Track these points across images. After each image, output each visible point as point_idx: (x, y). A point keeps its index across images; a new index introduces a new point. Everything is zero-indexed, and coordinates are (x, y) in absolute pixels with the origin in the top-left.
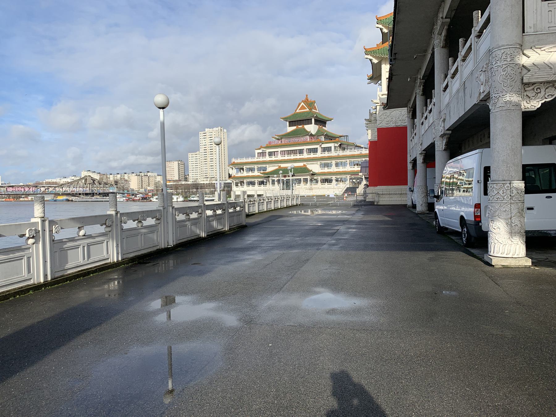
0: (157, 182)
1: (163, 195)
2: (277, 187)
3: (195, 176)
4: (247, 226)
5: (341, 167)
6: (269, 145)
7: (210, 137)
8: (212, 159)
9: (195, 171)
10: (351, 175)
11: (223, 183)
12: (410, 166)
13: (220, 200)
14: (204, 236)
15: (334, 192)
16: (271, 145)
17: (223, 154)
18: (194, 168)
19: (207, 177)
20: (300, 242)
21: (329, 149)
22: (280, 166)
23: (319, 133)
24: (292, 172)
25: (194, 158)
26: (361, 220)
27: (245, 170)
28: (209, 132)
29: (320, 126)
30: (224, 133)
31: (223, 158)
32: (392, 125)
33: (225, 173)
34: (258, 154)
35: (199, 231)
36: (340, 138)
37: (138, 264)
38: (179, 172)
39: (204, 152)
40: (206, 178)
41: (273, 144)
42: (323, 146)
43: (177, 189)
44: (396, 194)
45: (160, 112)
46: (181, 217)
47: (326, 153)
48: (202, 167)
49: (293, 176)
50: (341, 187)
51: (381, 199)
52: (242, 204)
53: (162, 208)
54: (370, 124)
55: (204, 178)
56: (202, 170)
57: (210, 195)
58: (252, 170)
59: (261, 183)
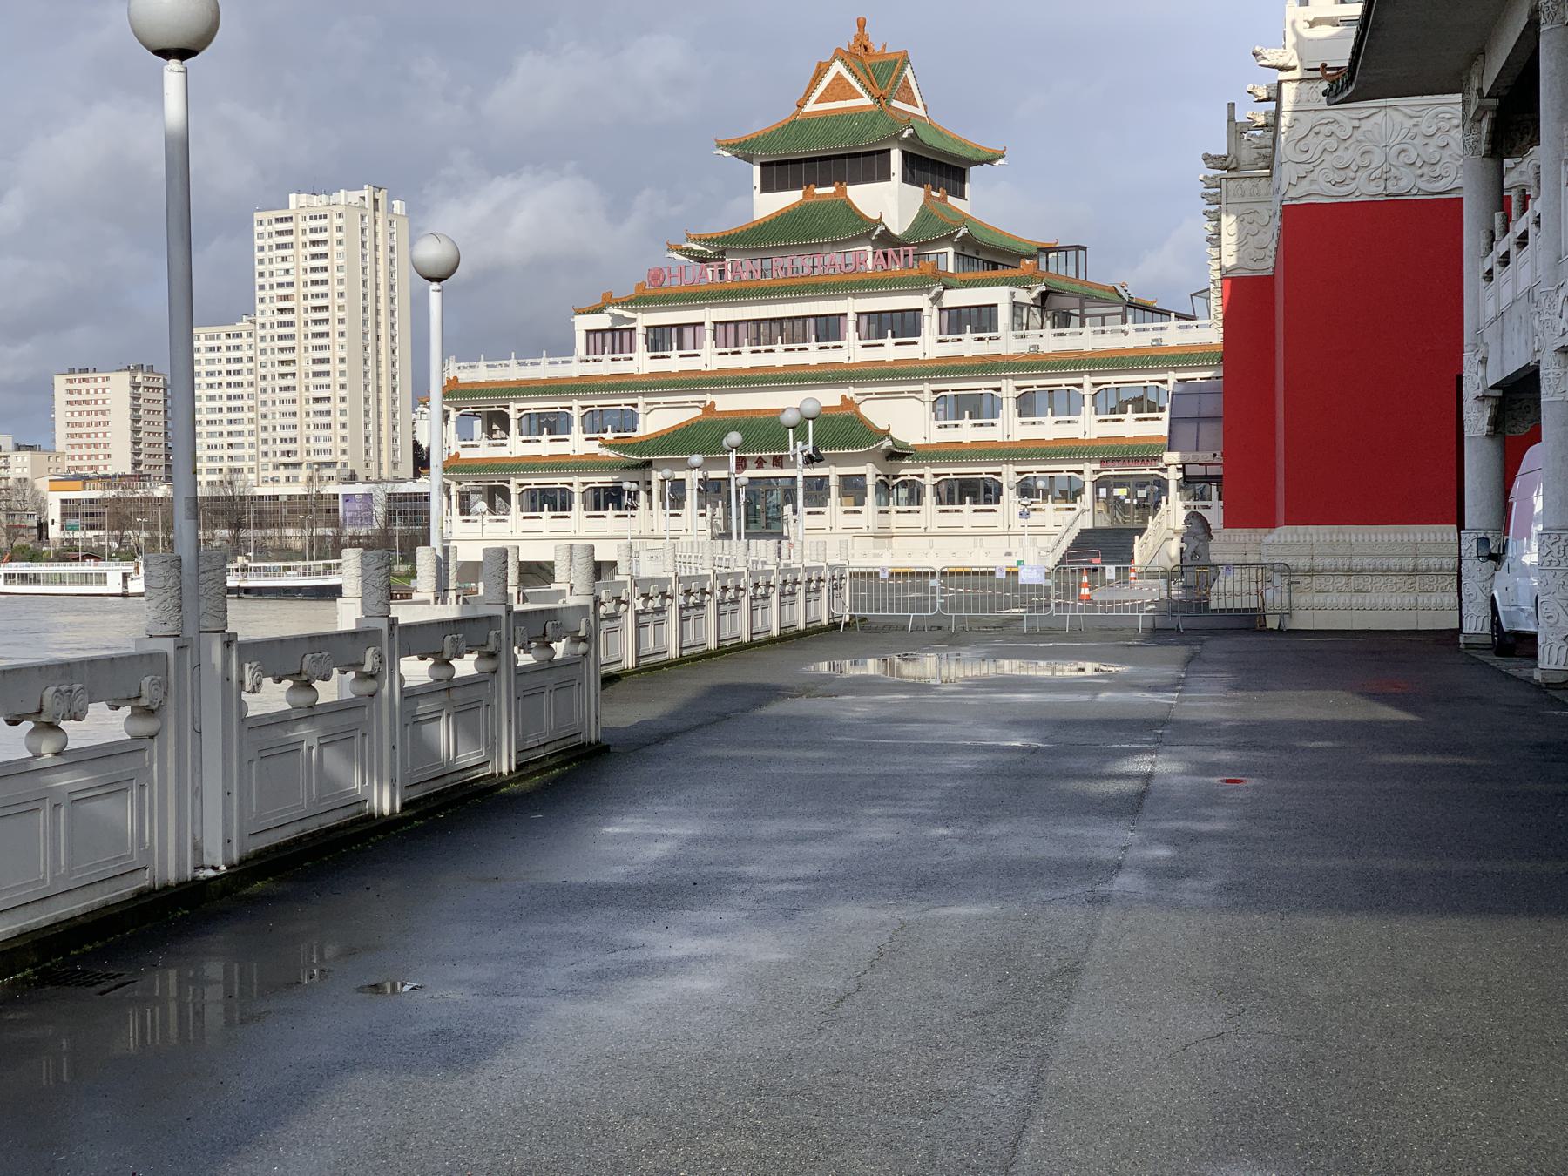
0: (11, 483)
1: (179, 568)
2: (693, 521)
3: (226, 452)
4: (606, 749)
5: (1049, 420)
6: (650, 291)
7: (314, 243)
8: (326, 361)
9: (226, 428)
10: (1102, 461)
11: (384, 498)
12: (1476, 420)
13: (446, 597)
14: (386, 810)
15: (1009, 554)
16: (661, 291)
17: (382, 338)
18: (221, 410)
19: (293, 459)
20: (964, 852)
21: (982, 319)
22: (713, 403)
23: (929, 231)
24: (806, 442)
25: (224, 354)
26: (1243, 716)
27: (513, 424)
28: (307, 213)
29: (934, 194)
30: (391, 223)
31: (383, 356)
32: (1365, 189)
33: (394, 440)
34: (592, 336)
35: (364, 782)
36: (1043, 260)
37: (40, 984)
38: (136, 431)
39: (281, 324)
40: (286, 465)
41: (676, 282)
42: (953, 298)
43: (122, 527)
44: (1386, 572)
45: (166, 73)
46: (271, 698)
47: (968, 336)
48: (264, 403)
49: (810, 460)
50: (1050, 528)
51: (1302, 600)
52: (584, 620)
53: (168, 646)
54: (1231, 183)
55: (276, 467)
56: (263, 422)
57: (311, 559)
58: (554, 424)
59: (609, 498)
